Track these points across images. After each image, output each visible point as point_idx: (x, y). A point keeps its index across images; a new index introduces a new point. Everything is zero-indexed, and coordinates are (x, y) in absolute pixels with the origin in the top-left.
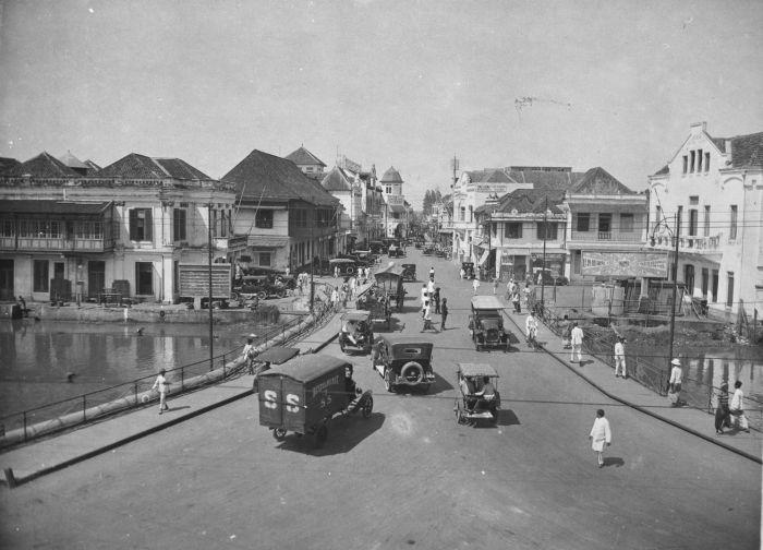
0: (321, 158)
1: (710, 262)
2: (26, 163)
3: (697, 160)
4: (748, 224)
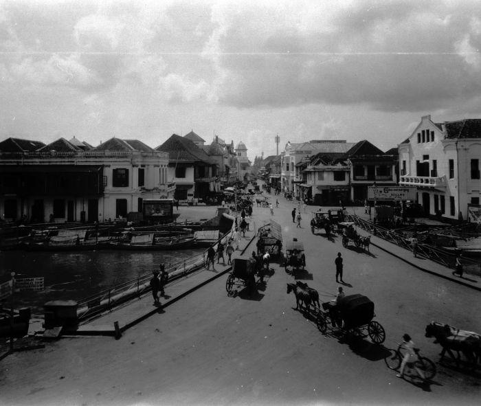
0: (203, 137)
1: (439, 191)
2: (99, 148)
3: (425, 136)
4: (162, 183)
